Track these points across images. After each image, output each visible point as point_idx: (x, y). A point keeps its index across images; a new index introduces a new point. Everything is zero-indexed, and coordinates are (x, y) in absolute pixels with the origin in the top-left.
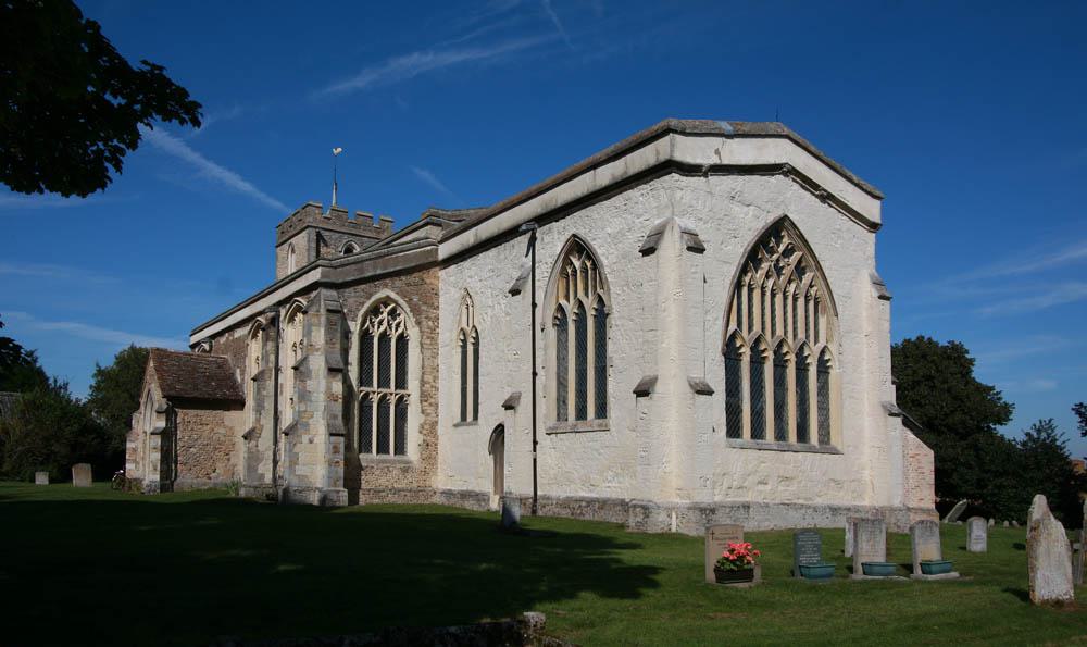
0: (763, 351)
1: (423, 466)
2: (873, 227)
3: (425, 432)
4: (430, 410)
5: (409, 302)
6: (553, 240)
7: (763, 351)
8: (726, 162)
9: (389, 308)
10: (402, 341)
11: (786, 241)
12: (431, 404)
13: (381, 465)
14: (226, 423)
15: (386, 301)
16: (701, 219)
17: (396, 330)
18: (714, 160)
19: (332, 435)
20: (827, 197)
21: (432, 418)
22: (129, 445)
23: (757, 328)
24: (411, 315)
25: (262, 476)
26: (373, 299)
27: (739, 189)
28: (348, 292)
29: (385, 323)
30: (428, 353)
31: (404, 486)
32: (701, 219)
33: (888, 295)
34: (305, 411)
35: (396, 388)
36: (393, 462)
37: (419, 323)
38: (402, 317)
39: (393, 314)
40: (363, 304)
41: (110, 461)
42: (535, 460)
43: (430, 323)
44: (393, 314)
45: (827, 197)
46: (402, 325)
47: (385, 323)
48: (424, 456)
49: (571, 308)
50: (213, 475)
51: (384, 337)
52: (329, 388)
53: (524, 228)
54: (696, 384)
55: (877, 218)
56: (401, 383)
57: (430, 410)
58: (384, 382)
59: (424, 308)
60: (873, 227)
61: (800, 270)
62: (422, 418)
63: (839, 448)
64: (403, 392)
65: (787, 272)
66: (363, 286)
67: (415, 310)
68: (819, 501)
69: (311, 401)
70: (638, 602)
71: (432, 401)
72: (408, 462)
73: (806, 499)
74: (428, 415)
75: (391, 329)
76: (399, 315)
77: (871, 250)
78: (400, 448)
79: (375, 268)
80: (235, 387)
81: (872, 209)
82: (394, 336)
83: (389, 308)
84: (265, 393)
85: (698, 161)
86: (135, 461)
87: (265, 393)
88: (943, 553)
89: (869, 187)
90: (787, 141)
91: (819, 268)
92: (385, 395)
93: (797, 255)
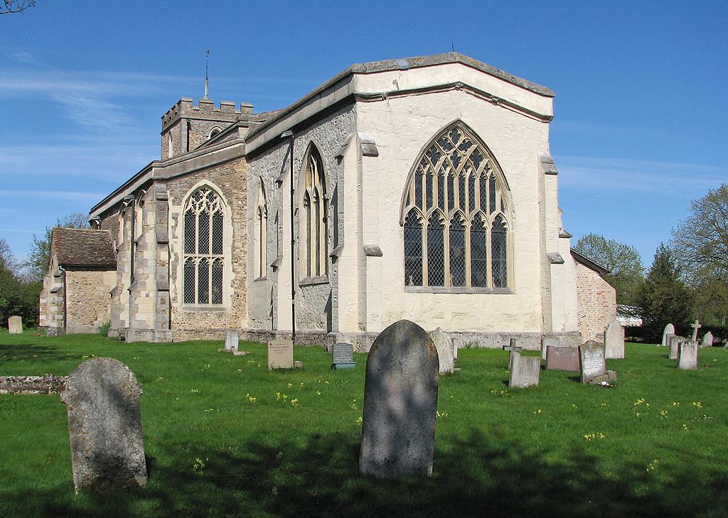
0: (463, 221)
1: (235, 311)
2: (545, 119)
3: (235, 286)
4: (240, 269)
5: (223, 188)
6: (301, 145)
7: (463, 221)
8: (402, 88)
9: (207, 193)
10: (219, 218)
11: (462, 138)
12: (240, 265)
13: (200, 312)
14: (105, 283)
15: (204, 188)
16: (382, 131)
17: (214, 209)
18: (393, 88)
19: (159, 290)
20: (497, 101)
21: (242, 275)
22: (42, 301)
23: (435, 205)
24: (224, 197)
25: (123, 322)
26: (194, 188)
27: (416, 105)
28: (174, 184)
29: (204, 205)
30: (238, 226)
31: (220, 327)
32: (382, 131)
33: (554, 171)
34: (143, 274)
35: (214, 253)
36: (211, 309)
37: (230, 203)
38: (218, 198)
39: (211, 197)
40: (186, 192)
41: (30, 316)
42: (293, 305)
43: (240, 202)
44: (211, 197)
45: (497, 101)
46: (218, 205)
47: (204, 205)
48: (235, 304)
49: (310, 190)
50: (95, 322)
51: (204, 215)
52: (157, 256)
53: (283, 135)
54: (370, 249)
55: (549, 112)
56: (218, 249)
57: (240, 269)
58: (204, 249)
59: (235, 191)
60: (545, 119)
61: (476, 158)
62: (233, 276)
63: (512, 290)
64: (218, 256)
65: (463, 161)
66: (186, 179)
67: (228, 193)
68: (491, 330)
69: (147, 266)
70: (479, 426)
71: (241, 261)
72: (222, 309)
73: (477, 329)
74: (238, 273)
75: (209, 208)
76: (216, 198)
77: (545, 136)
78: (218, 298)
79: (195, 164)
80: (111, 255)
81: (545, 106)
82: (212, 213)
83: (207, 193)
84: (125, 260)
85: (377, 91)
86: (45, 313)
87: (125, 260)
88: (12, 335)
89: (541, 89)
90: (459, 64)
91: (492, 155)
92: (204, 259)
93: (474, 147)
